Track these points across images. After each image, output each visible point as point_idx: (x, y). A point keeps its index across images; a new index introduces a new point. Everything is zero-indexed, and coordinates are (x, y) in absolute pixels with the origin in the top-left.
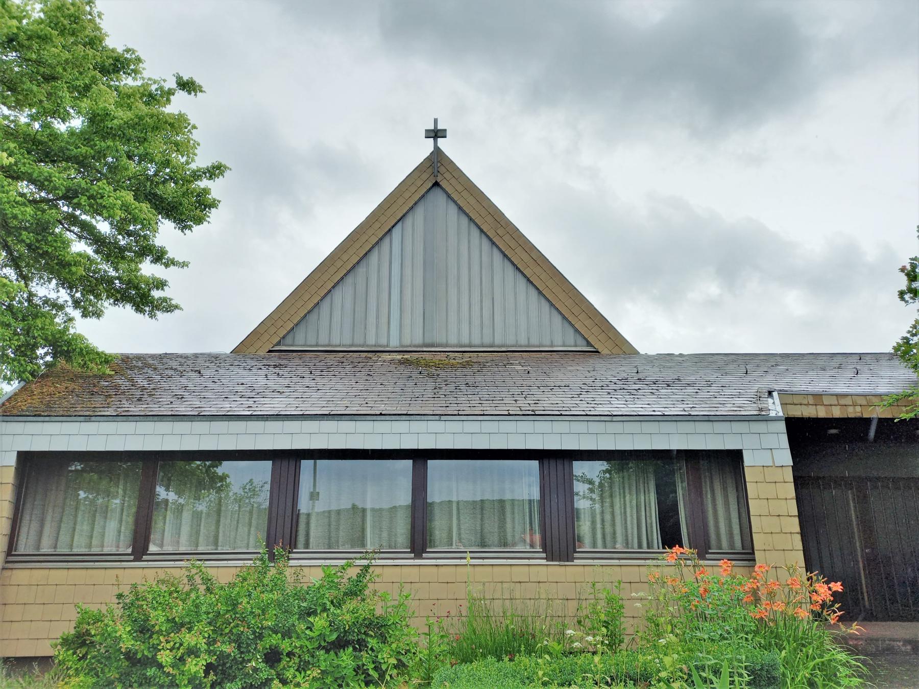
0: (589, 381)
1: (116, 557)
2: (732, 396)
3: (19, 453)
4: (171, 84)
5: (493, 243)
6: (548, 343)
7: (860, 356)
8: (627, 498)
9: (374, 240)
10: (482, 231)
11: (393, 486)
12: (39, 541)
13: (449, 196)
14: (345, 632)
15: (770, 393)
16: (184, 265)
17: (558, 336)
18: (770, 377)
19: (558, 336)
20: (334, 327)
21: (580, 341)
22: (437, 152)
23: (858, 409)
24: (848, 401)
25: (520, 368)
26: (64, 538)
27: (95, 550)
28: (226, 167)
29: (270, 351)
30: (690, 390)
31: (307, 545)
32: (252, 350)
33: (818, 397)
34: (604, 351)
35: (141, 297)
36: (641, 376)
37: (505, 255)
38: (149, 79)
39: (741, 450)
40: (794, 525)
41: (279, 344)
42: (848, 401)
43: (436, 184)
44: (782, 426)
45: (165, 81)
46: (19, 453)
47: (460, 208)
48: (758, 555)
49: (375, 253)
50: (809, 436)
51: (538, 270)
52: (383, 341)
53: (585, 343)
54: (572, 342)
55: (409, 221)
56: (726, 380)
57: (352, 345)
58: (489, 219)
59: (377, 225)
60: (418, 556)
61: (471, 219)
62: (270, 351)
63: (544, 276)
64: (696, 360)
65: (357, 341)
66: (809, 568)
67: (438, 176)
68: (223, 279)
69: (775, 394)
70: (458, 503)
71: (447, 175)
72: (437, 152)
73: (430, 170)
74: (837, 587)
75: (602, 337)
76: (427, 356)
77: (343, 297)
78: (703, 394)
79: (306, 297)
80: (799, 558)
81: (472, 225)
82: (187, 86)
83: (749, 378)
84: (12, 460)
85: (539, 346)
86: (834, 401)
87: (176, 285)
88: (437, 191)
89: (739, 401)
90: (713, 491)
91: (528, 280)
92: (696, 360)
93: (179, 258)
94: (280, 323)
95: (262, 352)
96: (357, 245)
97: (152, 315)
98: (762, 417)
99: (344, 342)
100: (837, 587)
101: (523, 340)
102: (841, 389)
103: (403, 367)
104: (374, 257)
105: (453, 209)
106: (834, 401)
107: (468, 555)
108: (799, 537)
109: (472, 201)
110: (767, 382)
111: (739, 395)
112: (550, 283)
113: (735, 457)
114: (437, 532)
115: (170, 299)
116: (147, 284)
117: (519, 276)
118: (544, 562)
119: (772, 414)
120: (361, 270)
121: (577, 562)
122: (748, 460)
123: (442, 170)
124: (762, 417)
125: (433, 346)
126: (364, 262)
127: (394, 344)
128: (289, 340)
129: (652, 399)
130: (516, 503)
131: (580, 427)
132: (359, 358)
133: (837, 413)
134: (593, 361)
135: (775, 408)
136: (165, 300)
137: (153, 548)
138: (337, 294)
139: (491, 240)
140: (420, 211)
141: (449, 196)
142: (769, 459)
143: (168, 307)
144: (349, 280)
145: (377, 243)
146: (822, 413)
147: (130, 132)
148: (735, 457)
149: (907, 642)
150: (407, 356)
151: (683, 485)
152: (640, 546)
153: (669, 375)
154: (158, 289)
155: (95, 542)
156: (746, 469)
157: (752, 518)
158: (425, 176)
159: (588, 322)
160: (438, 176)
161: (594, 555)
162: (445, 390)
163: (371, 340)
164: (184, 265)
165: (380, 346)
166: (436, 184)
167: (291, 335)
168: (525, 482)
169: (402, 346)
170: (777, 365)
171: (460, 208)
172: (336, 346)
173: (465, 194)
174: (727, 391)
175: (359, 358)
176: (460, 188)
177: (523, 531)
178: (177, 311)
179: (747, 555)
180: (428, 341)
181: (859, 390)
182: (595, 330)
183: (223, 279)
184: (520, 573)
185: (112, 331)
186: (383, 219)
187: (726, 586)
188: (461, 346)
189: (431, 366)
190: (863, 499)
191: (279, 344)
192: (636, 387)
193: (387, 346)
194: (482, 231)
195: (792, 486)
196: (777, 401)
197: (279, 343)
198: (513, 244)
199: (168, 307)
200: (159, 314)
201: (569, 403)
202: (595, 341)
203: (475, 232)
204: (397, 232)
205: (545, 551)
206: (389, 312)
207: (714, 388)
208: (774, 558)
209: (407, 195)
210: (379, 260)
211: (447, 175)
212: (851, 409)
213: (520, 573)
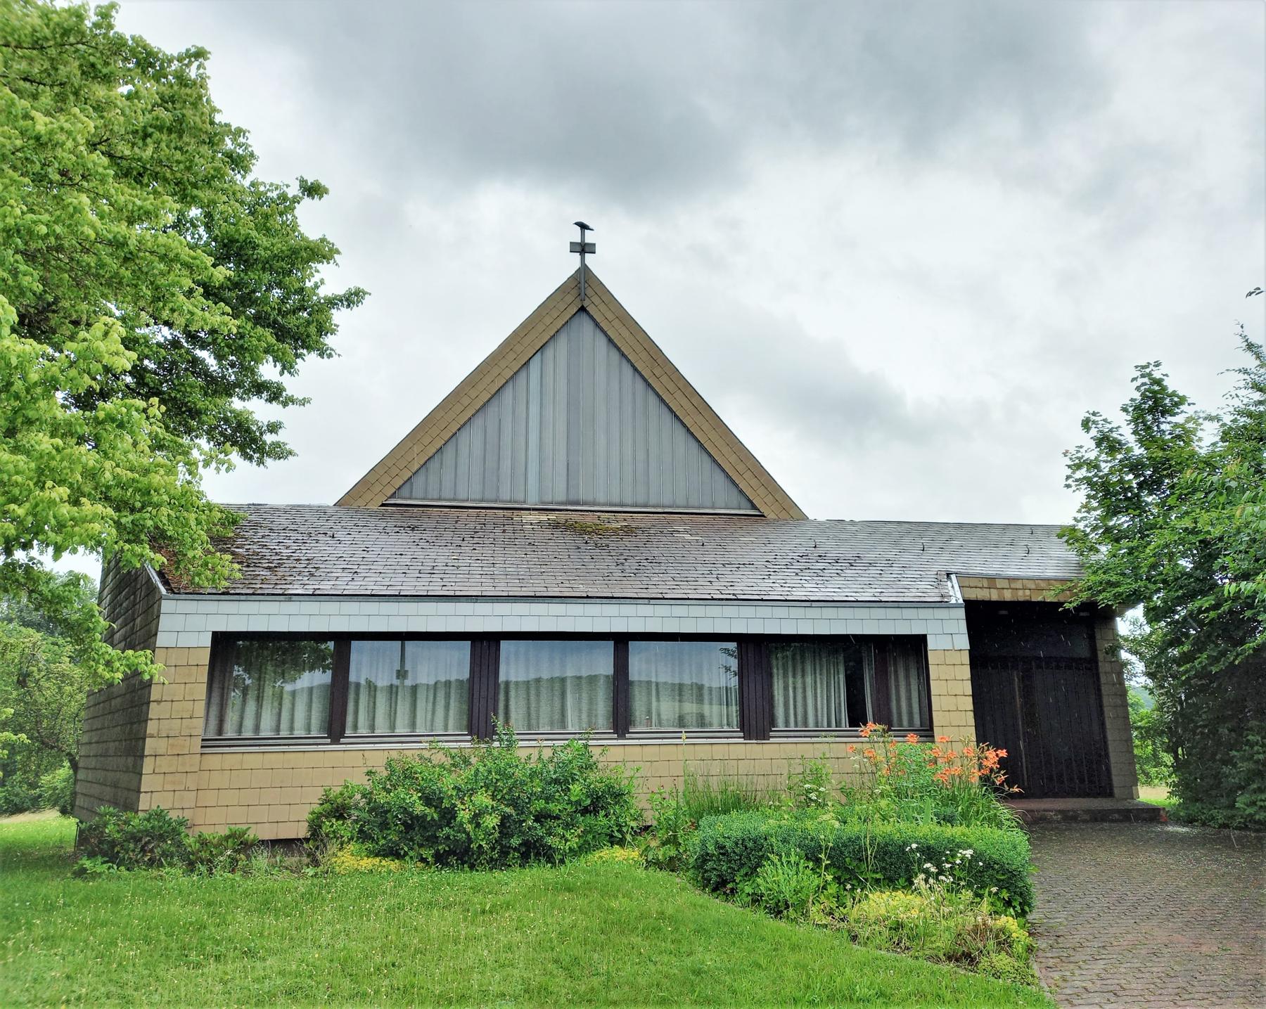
0: (770, 558)
1: (307, 740)
2: (914, 579)
3: (215, 634)
4: (293, 191)
5: (649, 385)
6: (709, 504)
7: (1032, 529)
8: (791, 680)
9: (509, 374)
10: (635, 369)
11: (455, 664)
13: (597, 325)
14: (598, 798)
15: (948, 575)
16: (303, 402)
17: (724, 500)
18: (946, 556)
19: (724, 500)
20: (462, 477)
21: (744, 503)
22: (584, 271)
23: (1028, 592)
24: (1019, 585)
25: (688, 537)
26: (249, 723)
27: (284, 734)
28: (365, 293)
29: (383, 505)
30: (873, 571)
32: (361, 502)
33: (992, 580)
34: (771, 516)
36: (820, 551)
37: (662, 400)
38: (271, 185)
39: (925, 636)
40: (968, 703)
41: (393, 496)
42: (1019, 585)
43: (583, 309)
44: (961, 613)
45: (288, 186)
46: (215, 634)
47: (610, 340)
48: (937, 731)
50: (982, 616)
51: (699, 419)
52: (521, 497)
53: (749, 505)
54: (735, 504)
55: (549, 352)
56: (906, 558)
57: (482, 501)
58: (644, 355)
59: (512, 356)
61: (623, 355)
62: (383, 505)
63: (705, 427)
64: (870, 530)
65: (488, 495)
66: (981, 737)
69: (953, 577)
70: (657, 684)
71: (596, 300)
72: (584, 271)
73: (575, 292)
74: (1003, 753)
75: (769, 499)
76: (575, 517)
77: (472, 441)
78: (887, 577)
79: (426, 440)
80: (971, 733)
81: (624, 361)
83: (925, 557)
84: (207, 641)
85: (699, 508)
86: (1005, 584)
87: (292, 425)
88: (584, 317)
89: (923, 585)
90: (896, 672)
91: (688, 430)
92: (870, 530)
93: (299, 395)
94: (395, 471)
95: (374, 506)
96: (488, 379)
97: (260, 462)
98: (943, 604)
99: (472, 496)
100: (1003, 753)
101: (681, 500)
102: (1012, 572)
103: (557, 533)
104: (508, 394)
105: (601, 342)
106: (1005, 584)
107: (684, 735)
108: (972, 714)
109: (626, 334)
110: (943, 562)
111: (921, 579)
112: (713, 435)
113: (921, 641)
114: (637, 713)
115: (285, 444)
116: (259, 428)
117: (678, 425)
118: (741, 740)
119: (953, 601)
120: (492, 410)
121: (772, 740)
122: (931, 644)
123: (589, 292)
124: (943, 604)
125: (577, 503)
126: (495, 402)
127: (532, 501)
128: (405, 491)
130: (512, 687)
131: (781, 612)
132: (495, 518)
133: (1008, 596)
134: (761, 529)
135: (956, 596)
136: (277, 445)
137: (348, 732)
138: (464, 437)
139: (645, 380)
140: (562, 340)
141: (597, 325)
142: (949, 642)
143: (280, 452)
144: (478, 422)
145: (512, 377)
146: (995, 596)
147: (276, 265)
148: (921, 641)
149: (1060, 812)
150: (552, 516)
151: (873, 670)
152: (829, 725)
153: (847, 551)
154: (271, 432)
155: (284, 724)
156: (929, 653)
157: (933, 698)
158: (569, 298)
159: (754, 482)
161: (787, 733)
162: (631, 565)
163: (505, 494)
164: (303, 402)
165: (515, 502)
166: (583, 309)
167: (408, 485)
168: (602, 662)
169: (543, 503)
170: (951, 539)
171: (610, 340)
172: (463, 501)
173: (616, 323)
174: (909, 574)
175: (495, 518)
176: (610, 316)
177: (721, 714)
178: (290, 457)
179: (927, 731)
180: (572, 498)
181: (1030, 573)
182: (762, 491)
183: (338, 417)
184: (719, 751)
185: (227, 483)
186: (519, 348)
187: (1222, 499)
188: (611, 505)
189: (584, 528)
190: (1026, 677)
191: (393, 496)
192: (821, 566)
193: (525, 502)
194: (635, 369)
195: (968, 668)
196: (956, 586)
197: (398, 494)
198: (671, 387)
199: (280, 452)
200: (269, 461)
202: (755, 502)
203: (628, 371)
205: (742, 730)
207: (895, 569)
208: (952, 734)
209: (548, 320)
210: (514, 398)
211: (596, 300)
212: (1020, 593)
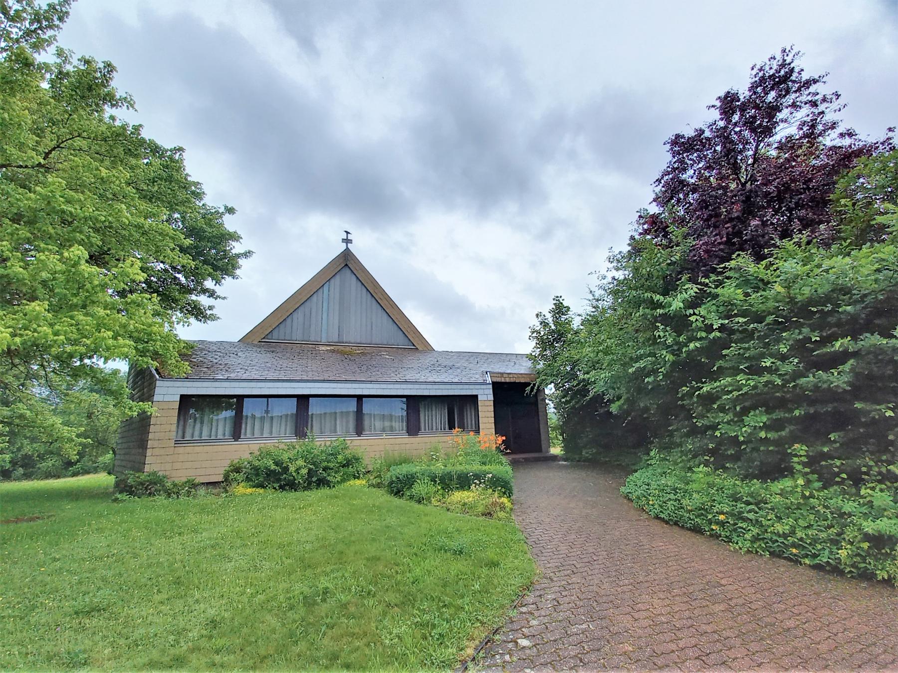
4: (222, 210)
12: (201, 433)
26: (197, 433)
30: (459, 371)
31: (245, 434)
34: (420, 349)
35: (198, 312)
40: (493, 420)
44: (491, 386)
49: (315, 295)
50: (498, 387)
55: (332, 281)
60: (359, 436)
67: (346, 262)
68: (238, 305)
74: (504, 438)
78: (464, 373)
82: (231, 211)
84: (178, 398)
87: (219, 307)
89: (477, 376)
95: (256, 342)
100: (504, 438)
104: (315, 298)
113: (475, 397)
122: (480, 398)
124: (484, 383)
127: (324, 341)
129: (446, 375)
133: (508, 380)
135: (489, 380)
140: (338, 277)
142: (486, 397)
148: (475, 397)
151: (458, 408)
158: (341, 261)
160: (346, 262)
183: (238, 305)
189: (348, 354)
197: (269, 336)
199: (213, 318)
200: (209, 322)
201: (417, 376)
204: (326, 288)
206: (325, 324)
213: (398, 441)
